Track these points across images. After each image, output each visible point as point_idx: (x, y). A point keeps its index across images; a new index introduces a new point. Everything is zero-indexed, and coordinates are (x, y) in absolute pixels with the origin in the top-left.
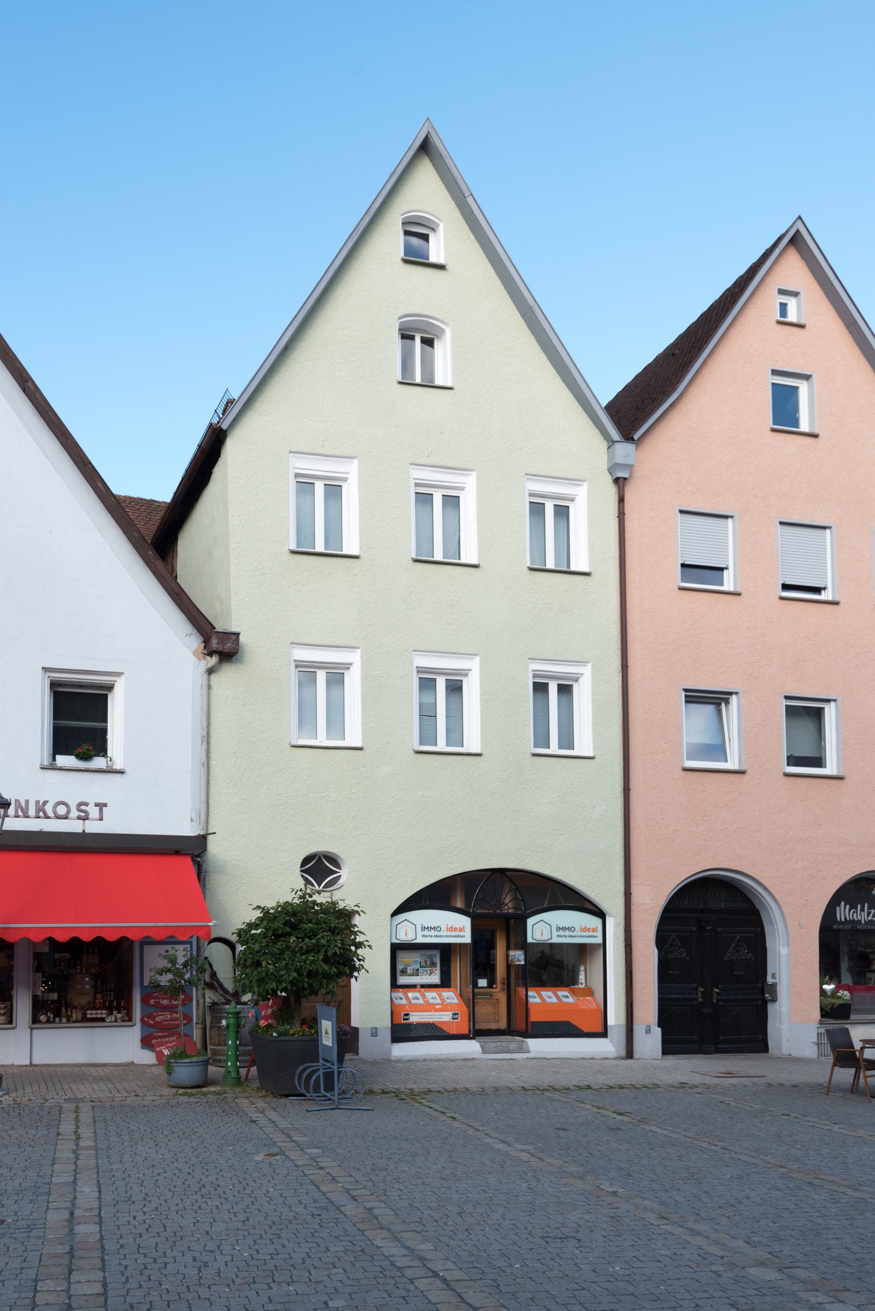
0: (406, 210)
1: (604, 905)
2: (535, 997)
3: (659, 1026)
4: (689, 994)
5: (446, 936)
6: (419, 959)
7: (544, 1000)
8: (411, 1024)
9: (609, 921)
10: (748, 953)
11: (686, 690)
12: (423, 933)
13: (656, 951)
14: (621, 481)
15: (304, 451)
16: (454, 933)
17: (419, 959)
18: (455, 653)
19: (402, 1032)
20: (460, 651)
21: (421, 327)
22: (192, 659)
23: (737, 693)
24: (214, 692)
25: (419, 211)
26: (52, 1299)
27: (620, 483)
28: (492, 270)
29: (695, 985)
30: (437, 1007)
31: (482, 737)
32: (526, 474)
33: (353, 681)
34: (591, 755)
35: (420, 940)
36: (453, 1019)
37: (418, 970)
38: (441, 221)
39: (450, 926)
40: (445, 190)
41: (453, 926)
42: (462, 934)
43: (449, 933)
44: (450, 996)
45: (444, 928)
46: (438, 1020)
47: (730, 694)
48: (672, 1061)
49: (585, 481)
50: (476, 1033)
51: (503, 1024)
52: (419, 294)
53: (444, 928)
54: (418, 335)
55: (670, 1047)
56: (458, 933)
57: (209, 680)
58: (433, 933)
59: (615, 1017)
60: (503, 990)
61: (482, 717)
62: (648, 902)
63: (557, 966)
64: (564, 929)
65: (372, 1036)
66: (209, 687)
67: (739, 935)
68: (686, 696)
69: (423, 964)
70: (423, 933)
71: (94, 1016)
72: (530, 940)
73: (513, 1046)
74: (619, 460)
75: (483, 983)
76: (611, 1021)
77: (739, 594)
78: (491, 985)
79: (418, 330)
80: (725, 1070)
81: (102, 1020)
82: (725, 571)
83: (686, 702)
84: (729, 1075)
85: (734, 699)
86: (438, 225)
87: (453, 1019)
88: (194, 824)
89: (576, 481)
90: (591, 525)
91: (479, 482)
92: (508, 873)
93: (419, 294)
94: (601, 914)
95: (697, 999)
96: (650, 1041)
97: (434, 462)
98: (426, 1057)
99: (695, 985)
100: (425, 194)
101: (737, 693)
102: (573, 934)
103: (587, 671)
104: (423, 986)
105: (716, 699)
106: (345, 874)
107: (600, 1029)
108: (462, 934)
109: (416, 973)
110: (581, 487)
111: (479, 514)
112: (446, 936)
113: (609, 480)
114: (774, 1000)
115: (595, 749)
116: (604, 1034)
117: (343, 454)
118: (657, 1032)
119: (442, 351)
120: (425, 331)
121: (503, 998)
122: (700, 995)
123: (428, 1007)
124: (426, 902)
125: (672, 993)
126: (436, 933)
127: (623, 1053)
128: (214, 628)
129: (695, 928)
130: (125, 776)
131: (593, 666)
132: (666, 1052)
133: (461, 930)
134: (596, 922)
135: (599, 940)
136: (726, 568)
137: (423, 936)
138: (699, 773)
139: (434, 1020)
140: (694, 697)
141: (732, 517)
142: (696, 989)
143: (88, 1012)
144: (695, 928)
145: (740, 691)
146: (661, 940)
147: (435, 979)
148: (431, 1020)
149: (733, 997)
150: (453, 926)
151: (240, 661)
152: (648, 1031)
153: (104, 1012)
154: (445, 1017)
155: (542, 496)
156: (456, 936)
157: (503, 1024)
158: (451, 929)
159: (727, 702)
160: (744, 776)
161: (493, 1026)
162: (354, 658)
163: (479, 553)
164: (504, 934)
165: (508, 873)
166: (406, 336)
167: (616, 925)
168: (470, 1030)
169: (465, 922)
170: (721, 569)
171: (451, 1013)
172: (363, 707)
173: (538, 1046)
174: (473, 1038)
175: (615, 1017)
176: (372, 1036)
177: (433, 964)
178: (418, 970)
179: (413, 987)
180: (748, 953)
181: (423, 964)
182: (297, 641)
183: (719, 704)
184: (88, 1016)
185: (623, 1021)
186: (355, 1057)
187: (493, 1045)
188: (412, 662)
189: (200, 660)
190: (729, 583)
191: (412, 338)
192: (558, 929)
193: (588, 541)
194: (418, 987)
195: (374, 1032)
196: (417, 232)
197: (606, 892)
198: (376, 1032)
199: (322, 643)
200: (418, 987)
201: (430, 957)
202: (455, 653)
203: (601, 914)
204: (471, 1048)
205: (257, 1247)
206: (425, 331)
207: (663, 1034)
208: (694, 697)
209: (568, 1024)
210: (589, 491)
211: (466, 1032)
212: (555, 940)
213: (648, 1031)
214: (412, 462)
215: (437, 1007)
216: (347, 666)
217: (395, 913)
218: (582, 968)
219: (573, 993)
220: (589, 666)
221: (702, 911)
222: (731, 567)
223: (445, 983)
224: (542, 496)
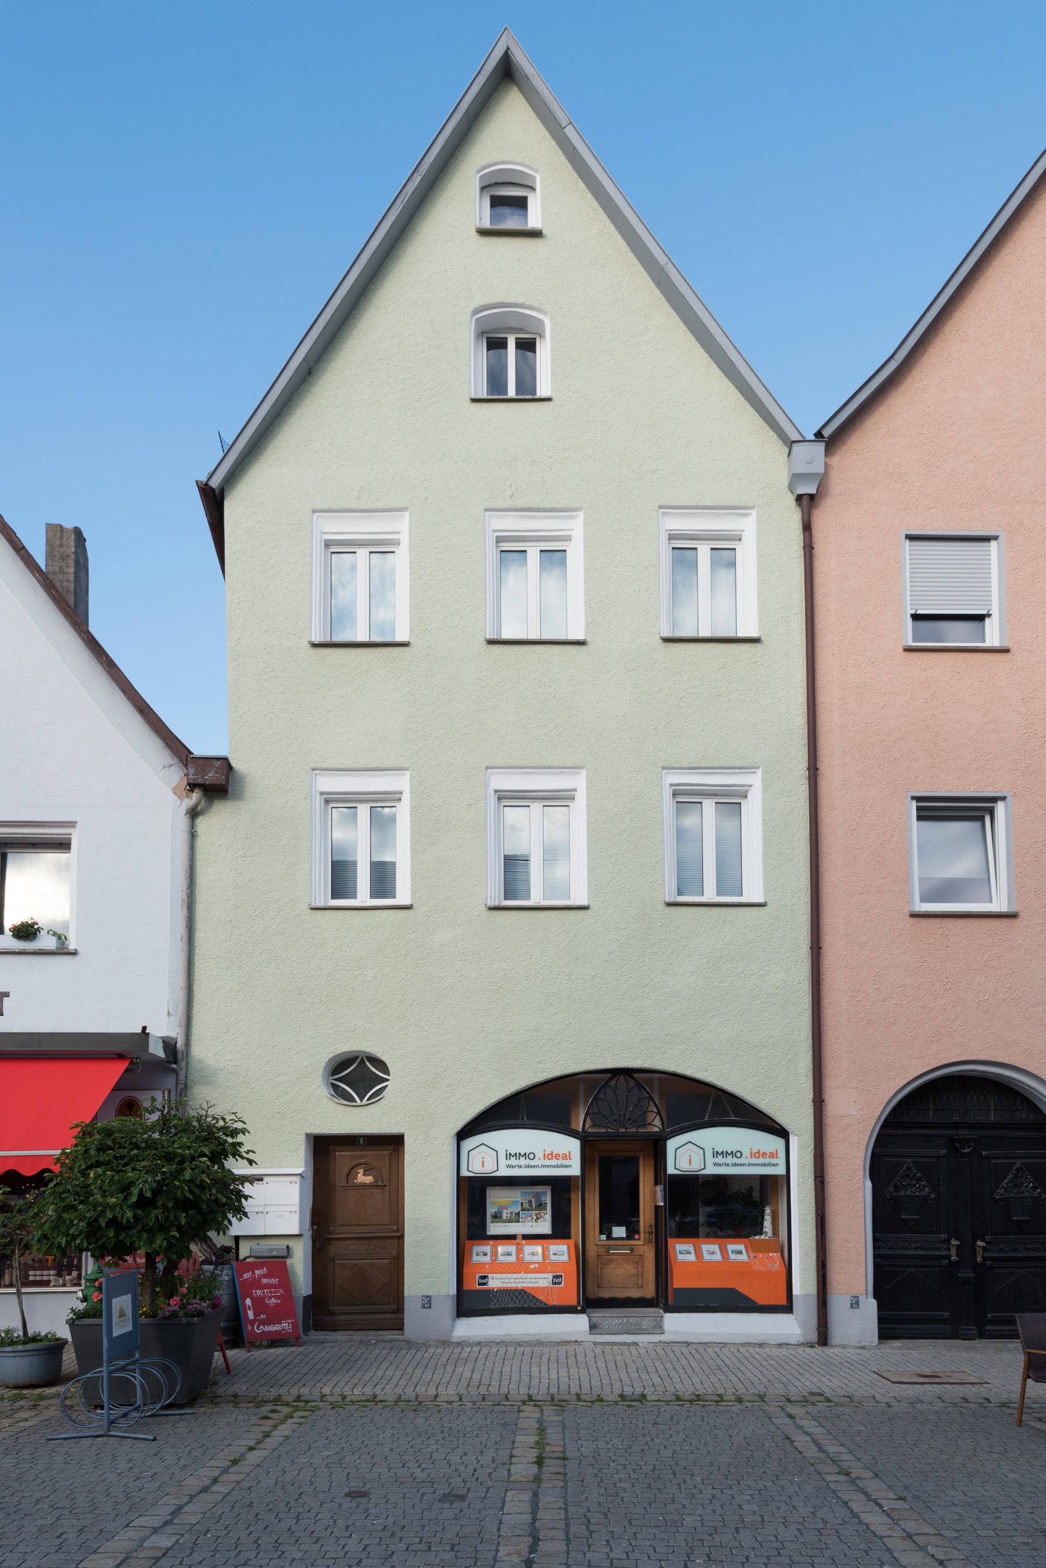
0: (487, 161)
1: (783, 1119)
2: (683, 1251)
3: (875, 1298)
4: (935, 1249)
5: (543, 1166)
6: (520, 1199)
7: (696, 1257)
8: (489, 1292)
9: (793, 1141)
10: (1035, 1188)
11: (918, 799)
12: (509, 1162)
13: (869, 1184)
14: (805, 500)
15: (334, 507)
16: (554, 1162)
17: (520, 1199)
18: (549, 767)
19: (471, 1302)
20: (556, 763)
21: (513, 323)
22: (172, 797)
23: (1004, 798)
24: (200, 842)
25: (504, 163)
26: (550, 1533)
27: (808, 503)
28: (613, 228)
29: (944, 1236)
30: (532, 1266)
31: (590, 883)
32: (660, 507)
33: (403, 812)
34: (762, 900)
35: (504, 1172)
36: (554, 1283)
37: (518, 1214)
38: (537, 171)
39: (755, 1150)
40: (542, 127)
41: (554, 1152)
42: (567, 1162)
43: (547, 1162)
44: (561, 1252)
45: (539, 1154)
46: (531, 1285)
47: (994, 800)
48: (896, 1348)
49: (752, 508)
50: (589, 1302)
51: (649, 1291)
52: (506, 275)
53: (539, 1154)
54: (507, 342)
55: (890, 1328)
56: (561, 1162)
57: (192, 826)
58: (523, 1161)
59: (803, 1283)
60: (650, 1241)
61: (589, 854)
62: (853, 1113)
63: (736, 1206)
64: (725, 1154)
65: (424, 1307)
66: (193, 835)
67: (1019, 1161)
68: (919, 809)
69: (526, 1206)
70: (509, 1162)
71: (38, 1278)
72: (671, 1170)
73: (646, 1323)
74: (802, 469)
75: (619, 1232)
76: (796, 1290)
77: (1007, 651)
78: (630, 1237)
79: (512, 330)
80: (927, 1371)
81: (46, 1284)
82: (987, 620)
83: (920, 818)
84: (932, 1378)
85: (1000, 808)
86: (534, 178)
87: (554, 1283)
88: (172, 1019)
89: (739, 509)
90: (762, 570)
91: (587, 525)
92: (636, 1075)
93: (506, 275)
94: (783, 1133)
95: (950, 1256)
96: (858, 1319)
97: (521, 503)
98: (505, 1339)
99: (944, 1236)
100: (513, 137)
101: (1004, 798)
102: (531, 1163)
103: (755, 781)
104: (526, 1237)
105: (975, 810)
106: (394, 1085)
107: (783, 1302)
108: (567, 1162)
109: (516, 1218)
110: (749, 518)
111: (586, 570)
112: (543, 1166)
113: (791, 500)
114: (54, 1335)
115: (767, 891)
116: (788, 1308)
117: (389, 506)
118: (870, 1306)
119: (544, 355)
120: (522, 330)
121: (649, 1254)
122: (953, 1251)
123: (521, 1266)
124: (523, 1118)
125: (906, 1248)
126: (528, 1162)
127: (814, 1337)
128: (191, 753)
129: (943, 1152)
130: (77, 958)
131: (764, 772)
132: (885, 1335)
133: (565, 1157)
134: (774, 1143)
135: (783, 1172)
136: (989, 615)
137: (508, 1166)
138: (938, 920)
139: (525, 1285)
140: (933, 810)
141: (996, 538)
142: (947, 1241)
143: (31, 1273)
144: (943, 1152)
145: (1009, 795)
146: (880, 1167)
147: (544, 1226)
148: (519, 1286)
149: (1011, 1254)
150: (554, 1152)
151: (238, 796)
152: (855, 1304)
153: (52, 1272)
154: (543, 1281)
155: (692, 538)
156: (765, 1165)
157: (649, 1291)
158: (551, 1156)
159: (991, 812)
160: (1017, 922)
161: (635, 1294)
162: (401, 783)
163: (587, 625)
164: (651, 1162)
165: (635, 1075)
166: (496, 344)
167: (801, 1148)
168: (579, 1303)
169: (573, 1146)
170: (981, 618)
171: (550, 1276)
172: (412, 849)
173: (680, 1325)
174: (583, 1311)
175: (803, 1283)
176: (424, 1307)
177: (541, 1206)
178: (518, 1214)
179: (511, 1238)
180: (1035, 1188)
181: (526, 1206)
182: (319, 765)
183: (982, 819)
184: (31, 1278)
185: (812, 1288)
186: (399, 1337)
187: (616, 1321)
188: (486, 784)
189: (181, 798)
190: (993, 635)
191: (502, 344)
192: (716, 1154)
193: (752, 594)
194: (519, 1238)
195: (427, 1302)
196: (507, 199)
197: (788, 1101)
198: (430, 1302)
199: (355, 766)
200: (519, 1238)
201: (537, 1196)
202: (549, 767)
203: (783, 1133)
204: (576, 1325)
205: (750, 1492)
206: (522, 330)
207: (879, 1310)
208: (933, 810)
209: (733, 1292)
210: (759, 521)
211: (573, 1302)
212: (711, 1170)
213: (855, 1304)
214: (487, 505)
215: (532, 1266)
216: (395, 797)
217: (464, 1133)
218: (768, 1211)
219: (753, 1248)
220: (759, 772)
221: (955, 1126)
222: (995, 612)
223: (560, 1230)
224: (692, 538)
